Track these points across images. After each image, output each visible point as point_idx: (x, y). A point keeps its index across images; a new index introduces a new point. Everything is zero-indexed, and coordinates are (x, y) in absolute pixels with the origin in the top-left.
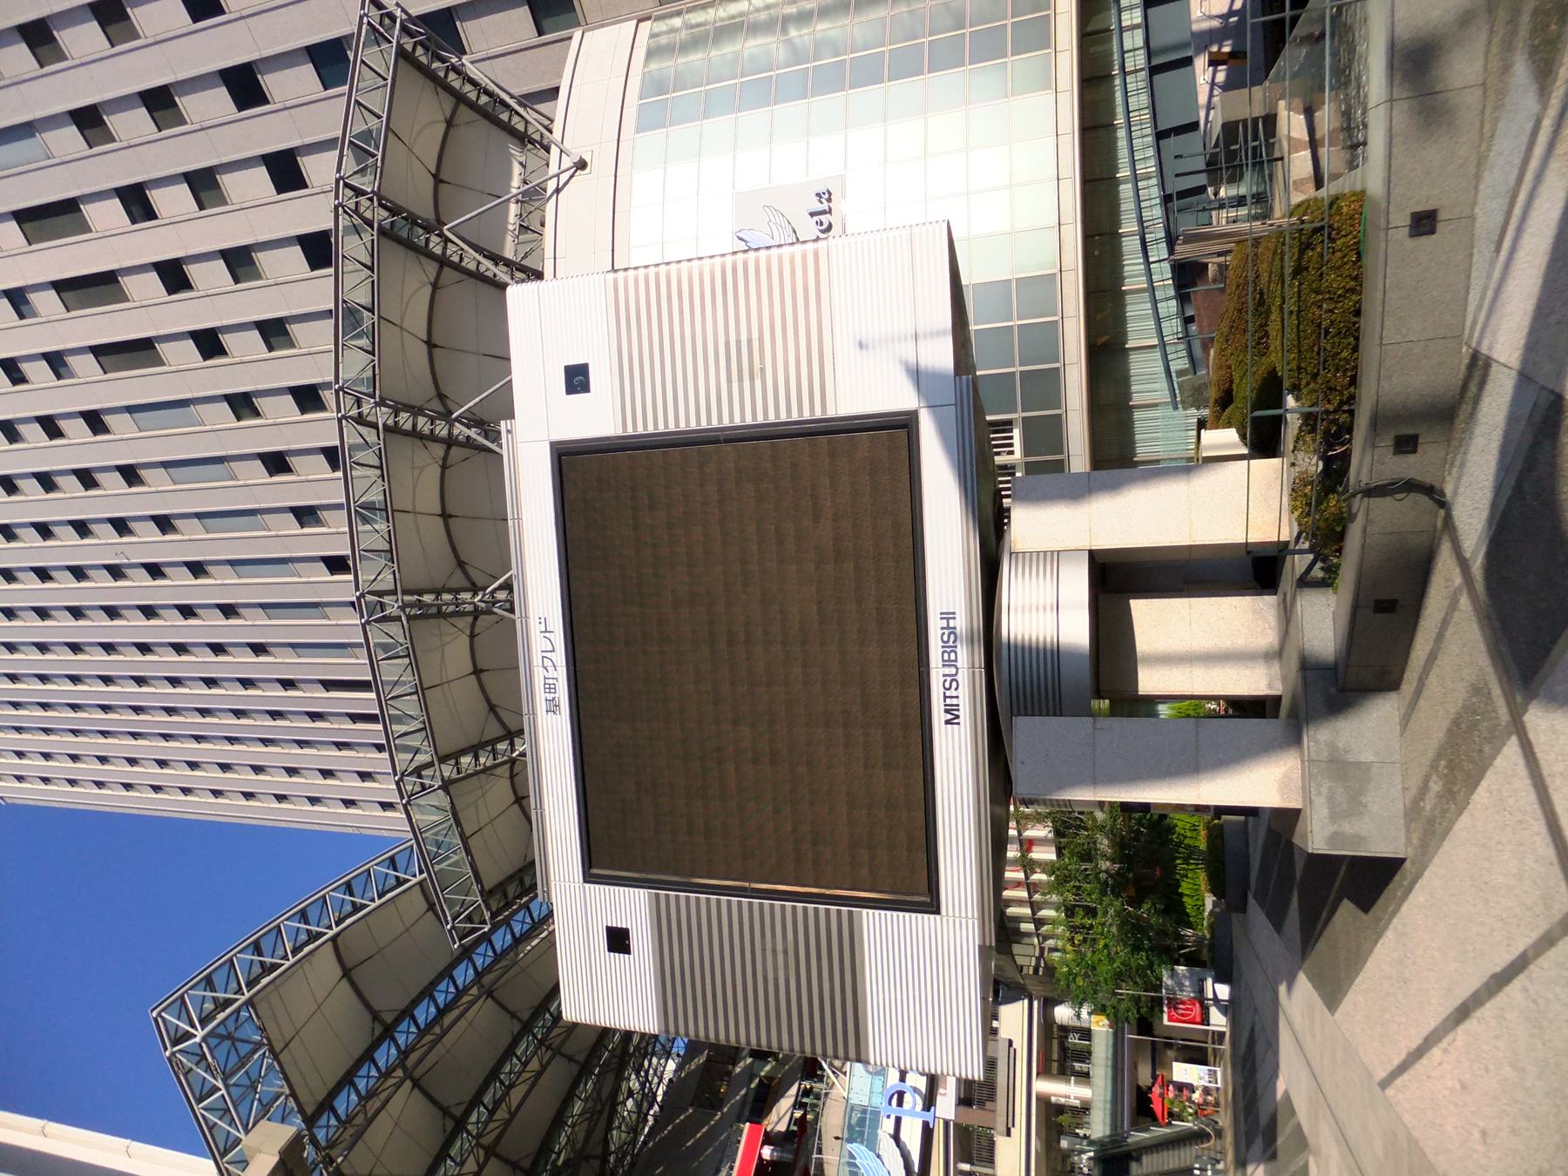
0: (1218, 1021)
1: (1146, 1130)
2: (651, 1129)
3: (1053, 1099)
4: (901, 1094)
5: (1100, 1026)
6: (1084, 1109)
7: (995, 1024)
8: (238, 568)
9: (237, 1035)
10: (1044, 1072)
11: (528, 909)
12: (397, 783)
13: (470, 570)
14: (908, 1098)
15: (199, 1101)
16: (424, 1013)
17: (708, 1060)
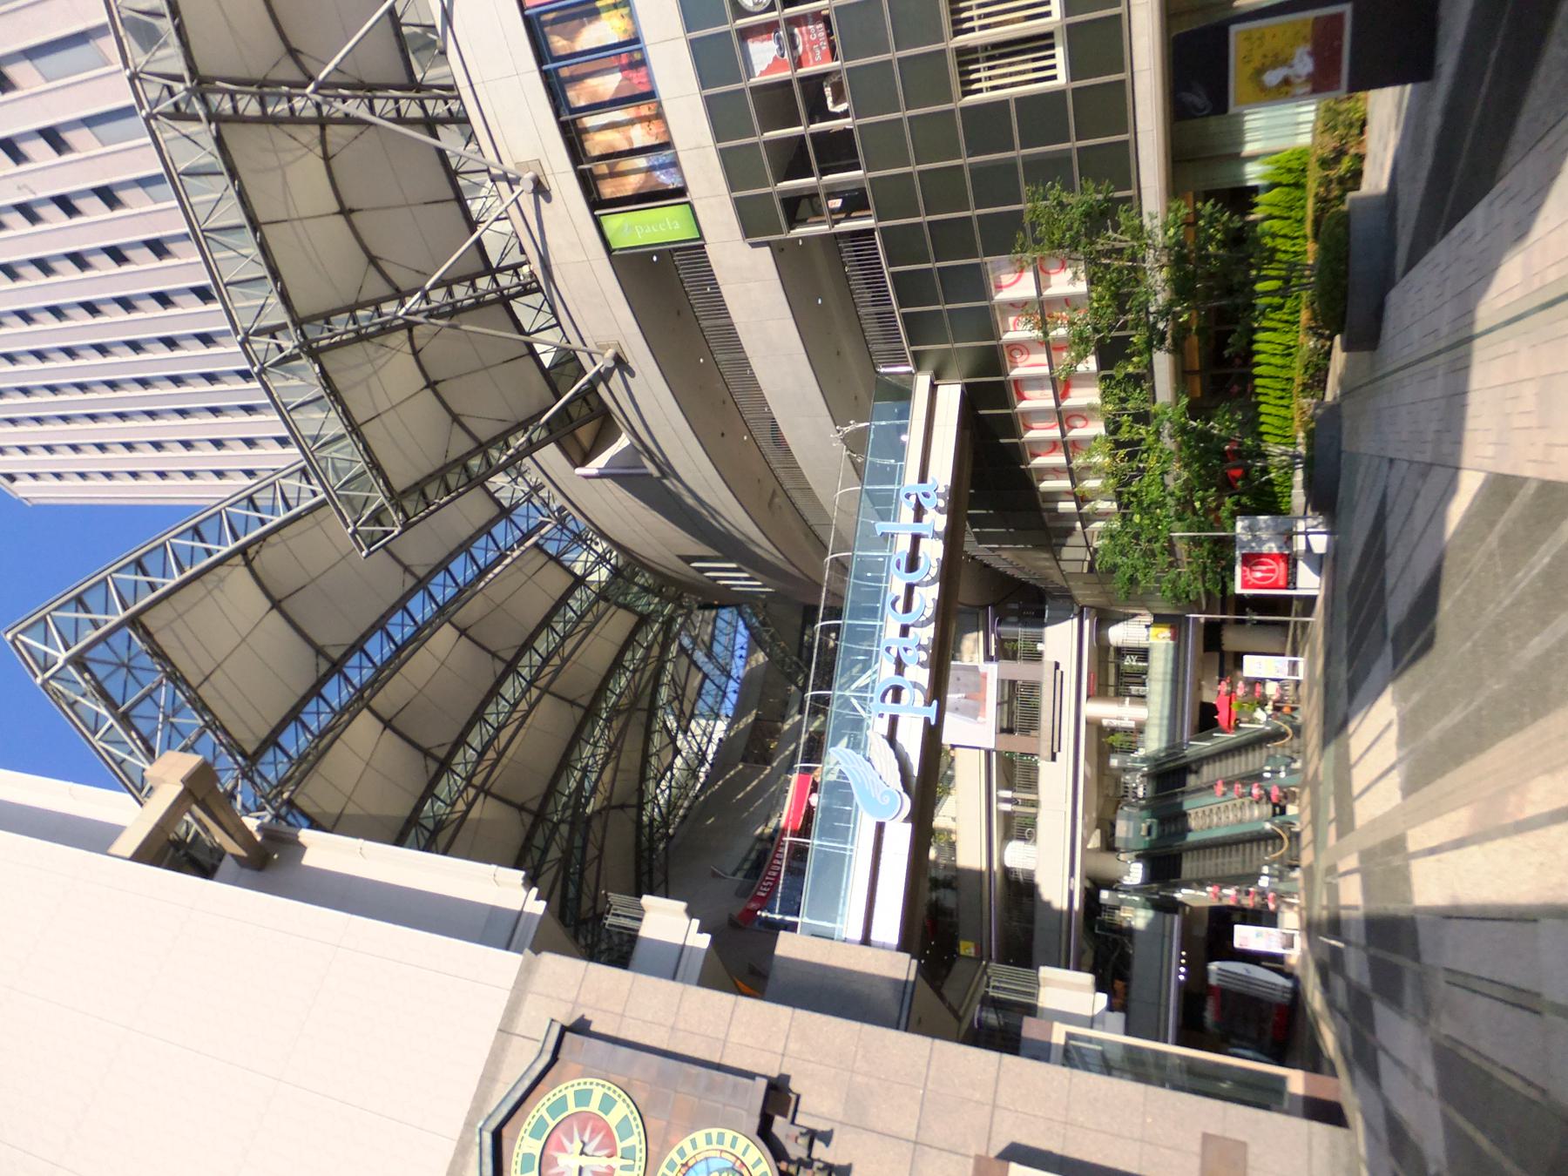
0: (1309, 582)
1: (1211, 738)
2: (703, 785)
3: (1105, 722)
4: (897, 691)
5: (1160, 640)
6: (1140, 729)
7: (1040, 647)
8: (151, 189)
9: (132, 663)
10: (1099, 691)
11: (489, 534)
12: (242, 344)
13: (303, 59)
14: (905, 695)
15: (95, 733)
16: (378, 648)
17: (757, 719)
